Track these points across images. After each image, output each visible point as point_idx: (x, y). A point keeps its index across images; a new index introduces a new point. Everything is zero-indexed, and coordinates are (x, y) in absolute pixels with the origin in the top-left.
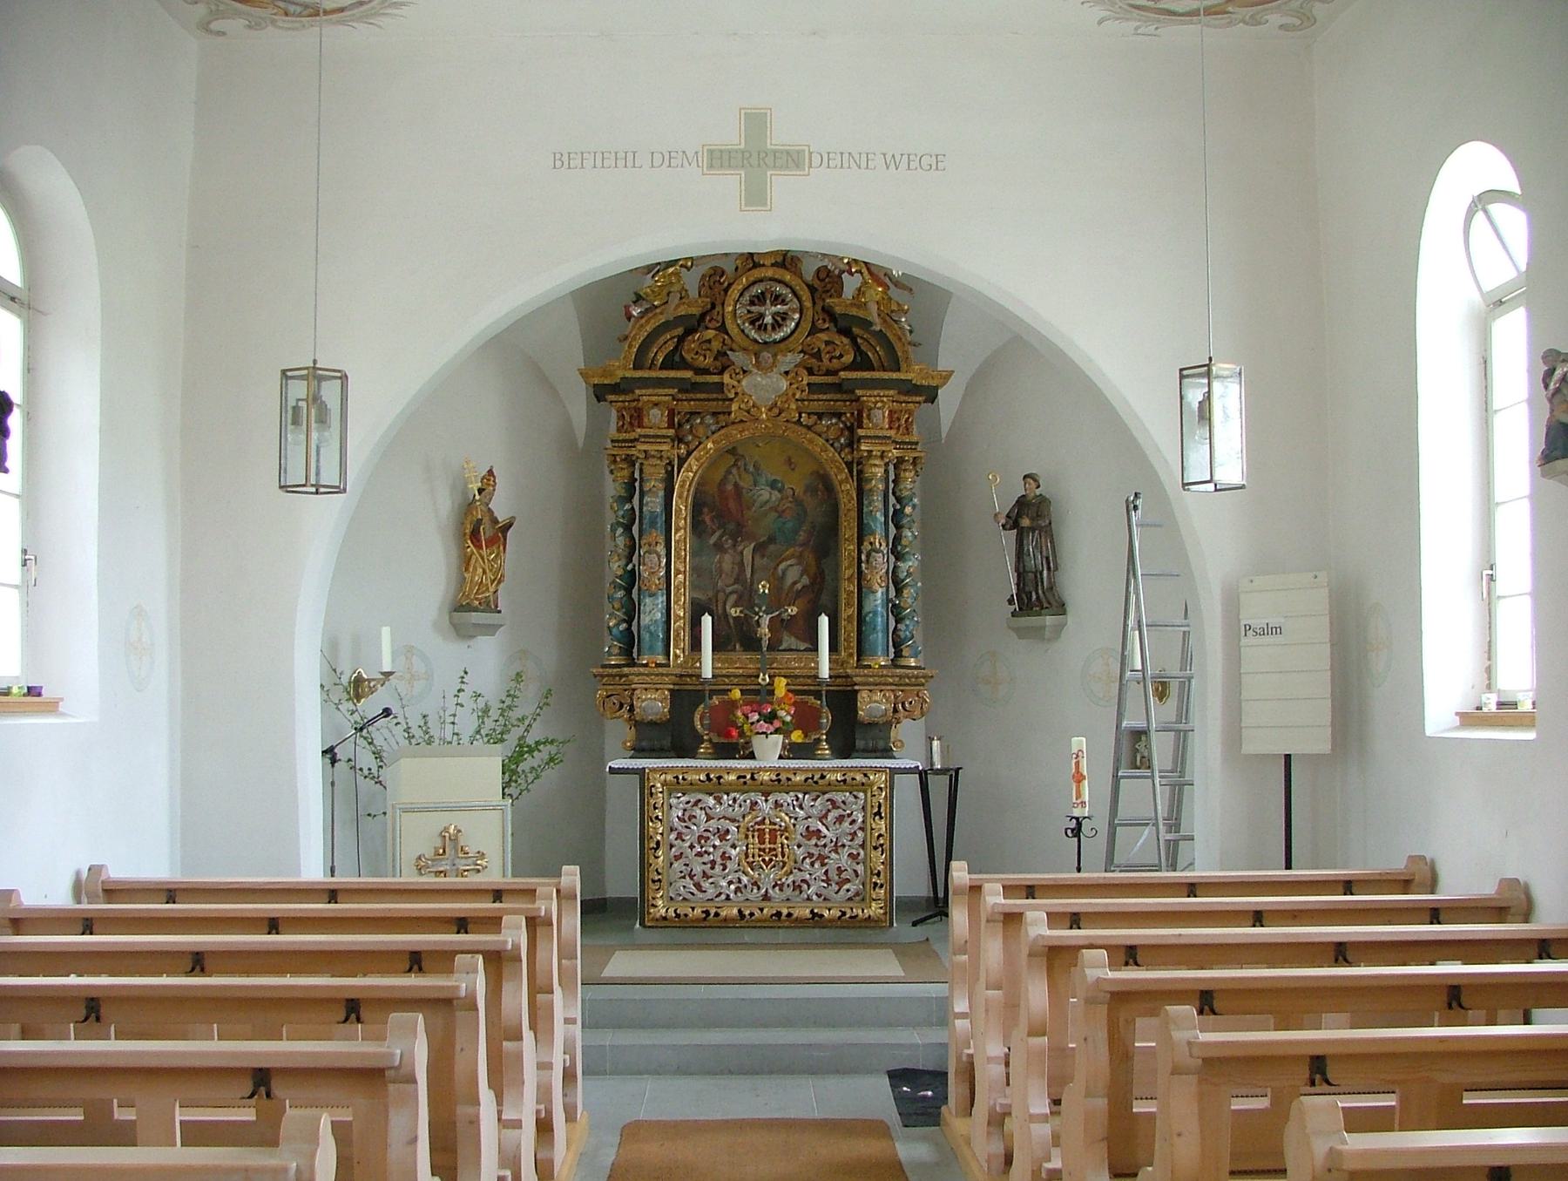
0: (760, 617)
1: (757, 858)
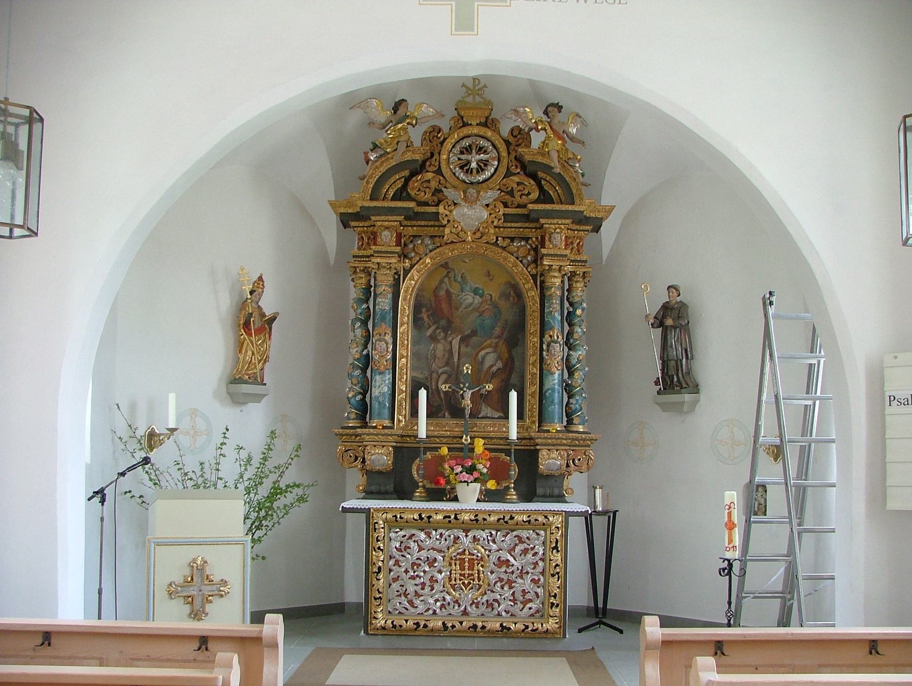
0: (464, 391)
1: (458, 582)
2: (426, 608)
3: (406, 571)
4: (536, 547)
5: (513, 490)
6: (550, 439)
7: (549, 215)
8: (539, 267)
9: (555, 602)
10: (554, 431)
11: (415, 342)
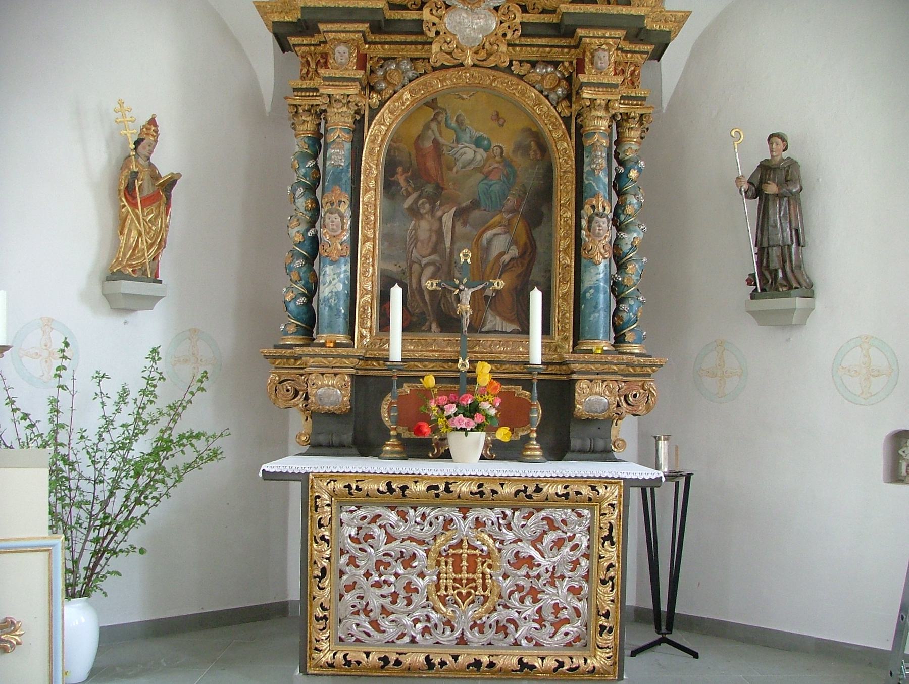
0: (461, 291)
1: (451, 591)
2: (400, 633)
3: (367, 575)
4: (577, 535)
5: (535, 443)
6: (593, 363)
7: (593, 22)
8: (574, 106)
9: (605, 624)
10: (600, 352)
11: (387, 219)
